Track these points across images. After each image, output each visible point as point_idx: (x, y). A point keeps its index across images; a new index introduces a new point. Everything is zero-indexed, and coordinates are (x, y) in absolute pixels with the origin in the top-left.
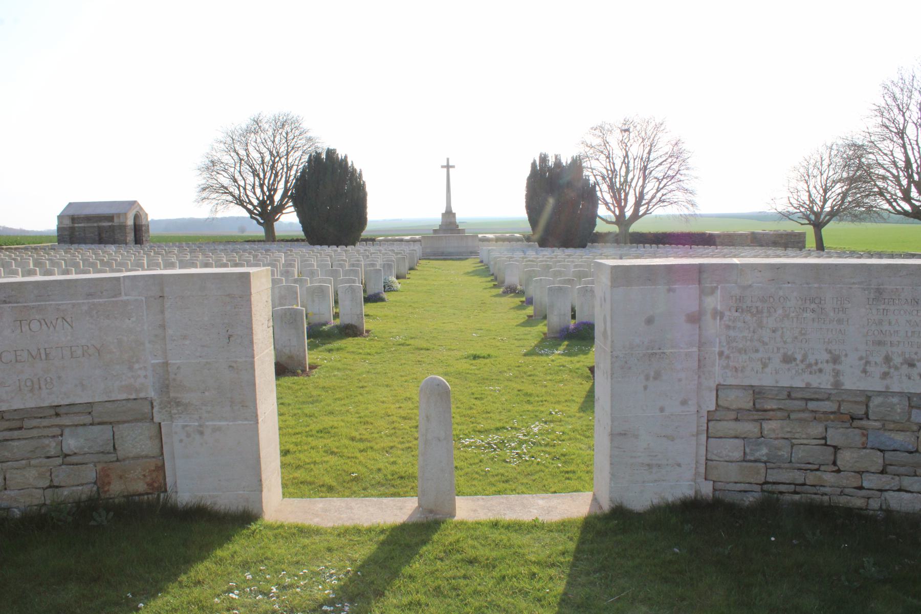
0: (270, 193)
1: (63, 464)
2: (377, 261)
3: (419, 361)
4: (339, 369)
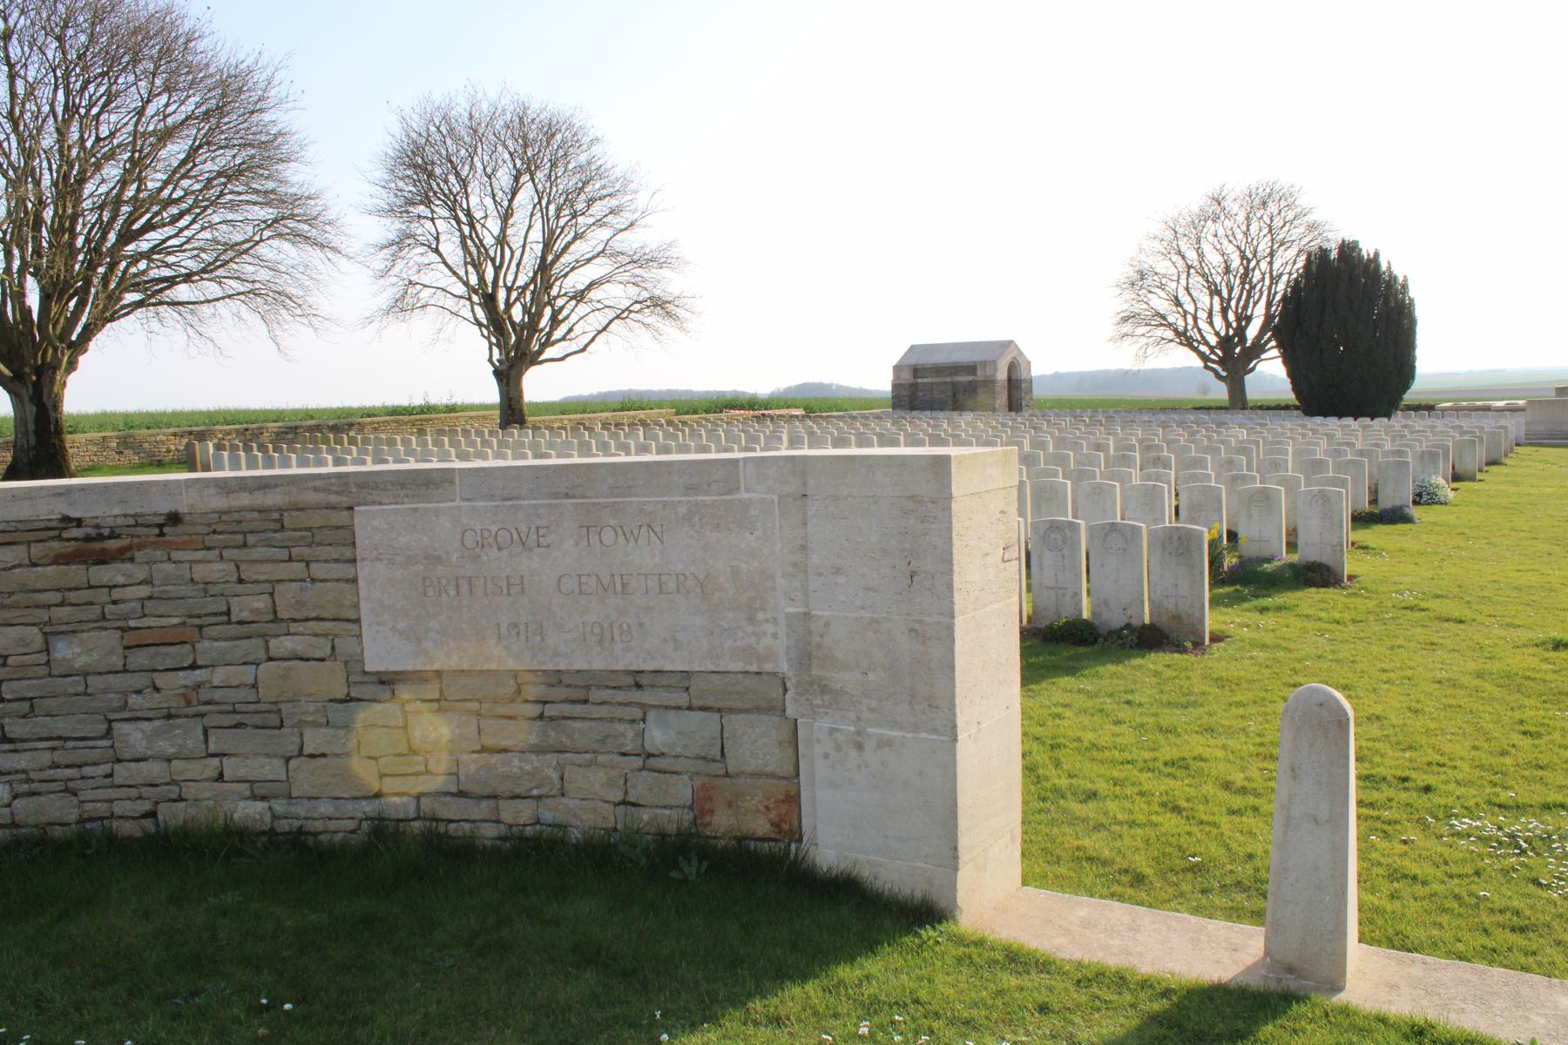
1: (643, 768)
2: (1318, 444)
3: (1433, 644)
4: (1264, 647)
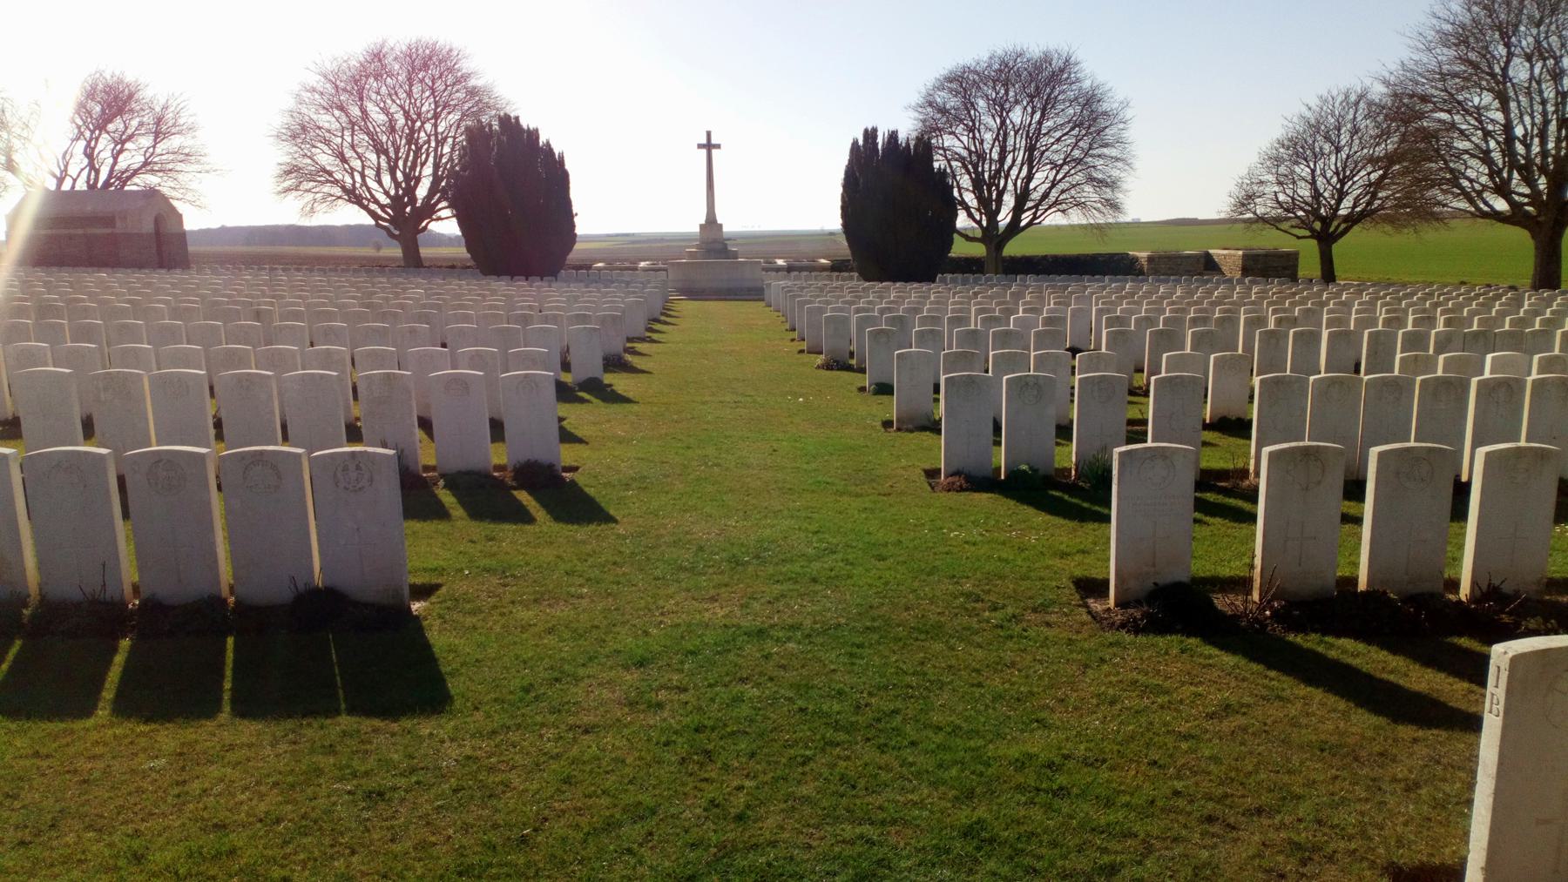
0: (408, 184)
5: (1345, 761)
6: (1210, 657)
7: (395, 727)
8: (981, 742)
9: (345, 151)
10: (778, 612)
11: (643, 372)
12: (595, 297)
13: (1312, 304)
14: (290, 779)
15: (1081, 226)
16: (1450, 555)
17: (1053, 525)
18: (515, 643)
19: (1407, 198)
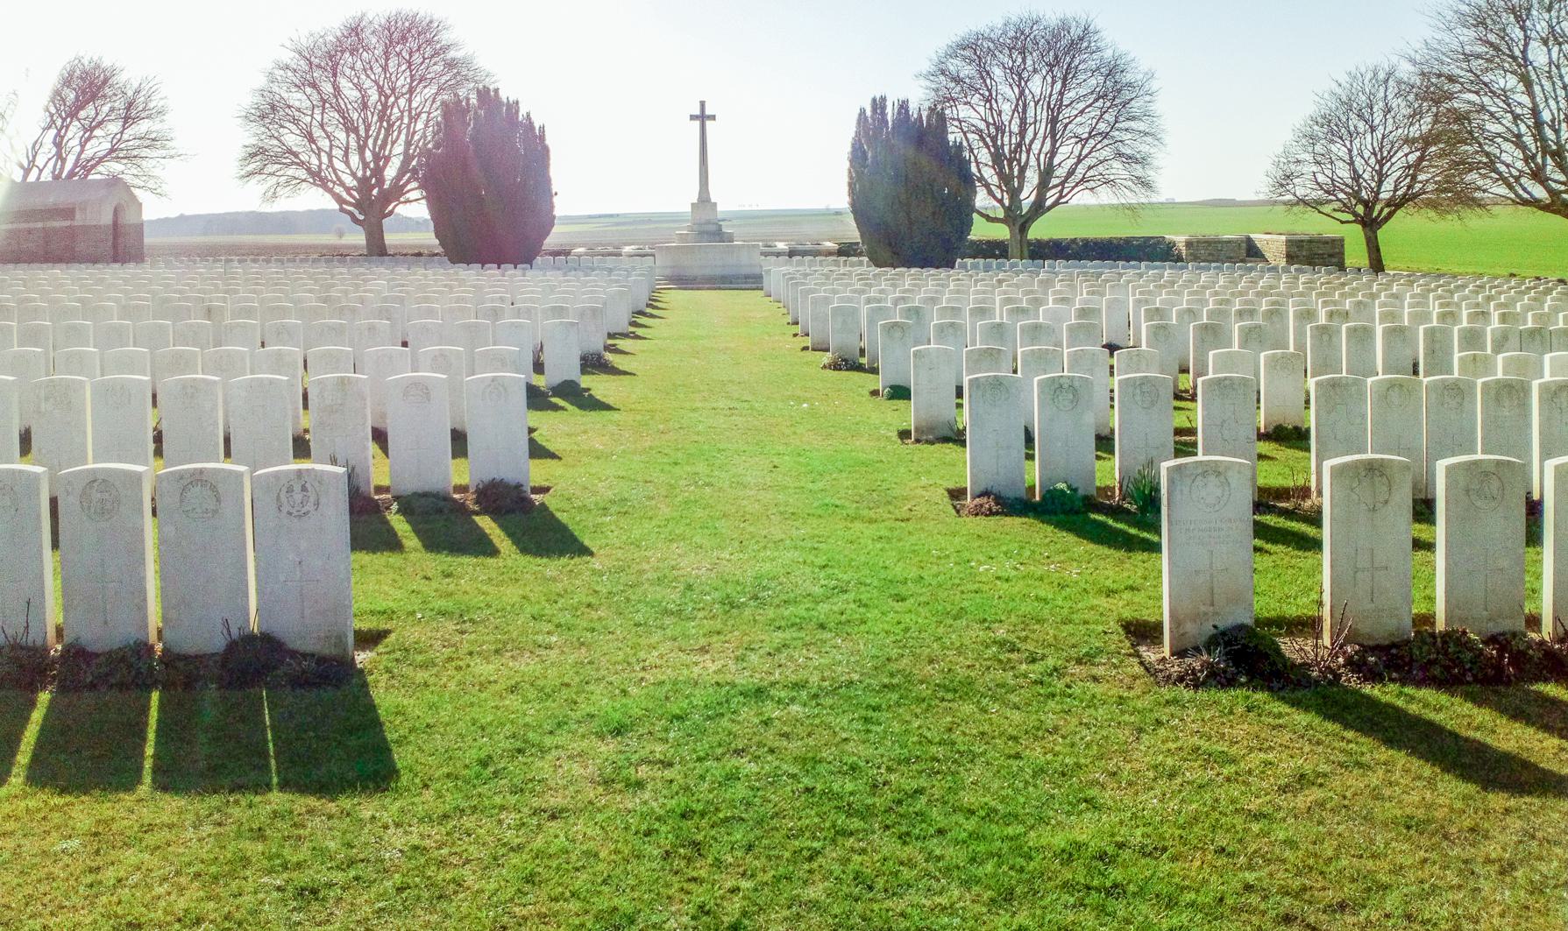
5: (1433, 840)
6: (1280, 716)
7: (332, 807)
8: (1020, 829)
9: (314, 130)
10: (780, 666)
11: (625, 373)
12: (573, 286)
13: (1363, 296)
14: (213, 869)
15: (1112, 207)
16: (1528, 585)
17: (1097, 556)
18: (472, 704)
19: (1447, 182)
